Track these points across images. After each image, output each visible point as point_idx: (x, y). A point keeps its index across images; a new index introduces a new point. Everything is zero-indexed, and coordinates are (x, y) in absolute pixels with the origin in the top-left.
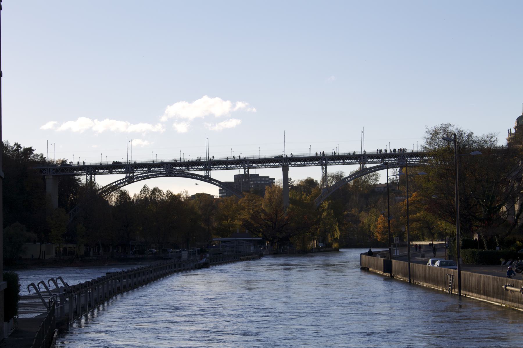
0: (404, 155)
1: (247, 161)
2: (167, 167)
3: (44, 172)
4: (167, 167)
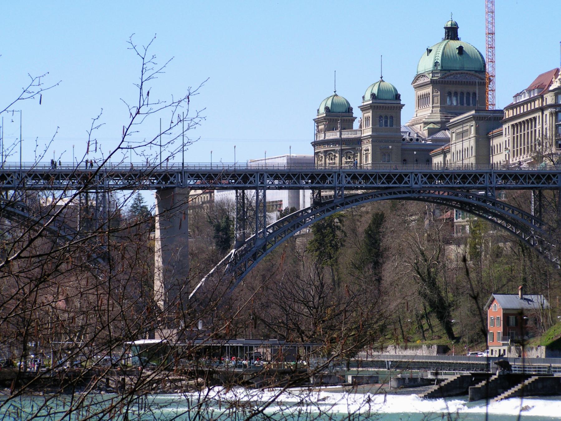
0: (416, 175)
1: (265, 174)
2: (416, 178)
3: (251, 179)
4: (416, 178)
